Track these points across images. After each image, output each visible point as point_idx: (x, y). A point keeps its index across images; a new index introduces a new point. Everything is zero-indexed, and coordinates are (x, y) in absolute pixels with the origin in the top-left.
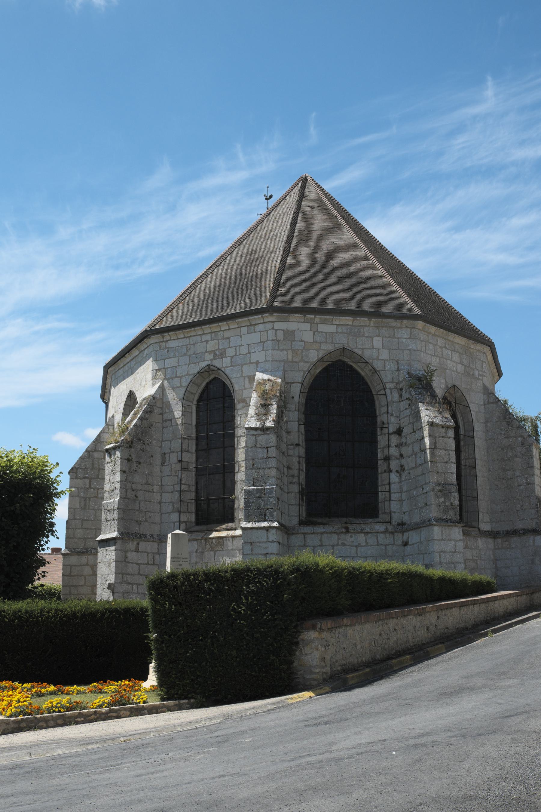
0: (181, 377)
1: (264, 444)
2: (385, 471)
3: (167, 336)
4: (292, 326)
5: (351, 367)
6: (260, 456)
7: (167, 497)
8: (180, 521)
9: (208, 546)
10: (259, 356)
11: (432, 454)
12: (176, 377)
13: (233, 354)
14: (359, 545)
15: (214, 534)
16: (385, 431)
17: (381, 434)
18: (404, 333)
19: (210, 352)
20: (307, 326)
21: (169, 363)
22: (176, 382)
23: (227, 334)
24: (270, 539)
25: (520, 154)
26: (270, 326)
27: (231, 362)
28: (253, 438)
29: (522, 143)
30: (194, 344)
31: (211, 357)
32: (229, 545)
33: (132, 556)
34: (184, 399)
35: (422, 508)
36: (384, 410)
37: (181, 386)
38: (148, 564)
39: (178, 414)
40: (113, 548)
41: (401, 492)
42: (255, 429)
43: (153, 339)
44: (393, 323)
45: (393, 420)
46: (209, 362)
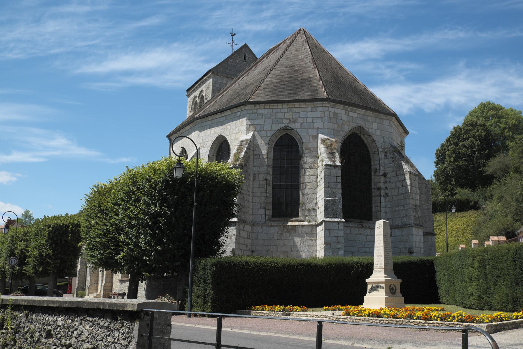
0: (266, 131)
1: (335, 174)
2: (378, 196)
3: (258, 106)
4: (337, 111)
5: (360, 137)
6: (333, 181)
7: (257, 200)
8: (265, 214)
9: (286, 230)
10: (318, 124)
11: (411, 188)
12: (263, 130)
13: (303, 122)
14: (367, 235)
15: (289, 224)
16: (378, 174)
17: (375, 175)
18: (386, 122)
19: (287, 119)
20: (343, 112)
21: (257, 122)
22: (264, 133)
23: (298, 110)
24: (340, 228)
25: (248, 27)
26: (326, 109)
27: (301, 126)
28: (329, 171)
29: (250, 22)
30: (276, 113)
31: (288, 121)
32: (300, 230)
33: (242, 232)
34: (268, 144)
35: (402, 217)
36: (376, 162)
37: (267, 136)
38: (247, 238)
39: (264, 151)
40: (234, 228)
41: (252, 202)
42: (330, 166)
43: (249, 107)
44: (382, 116)
45: (382, 168)
46: (286, 125)
